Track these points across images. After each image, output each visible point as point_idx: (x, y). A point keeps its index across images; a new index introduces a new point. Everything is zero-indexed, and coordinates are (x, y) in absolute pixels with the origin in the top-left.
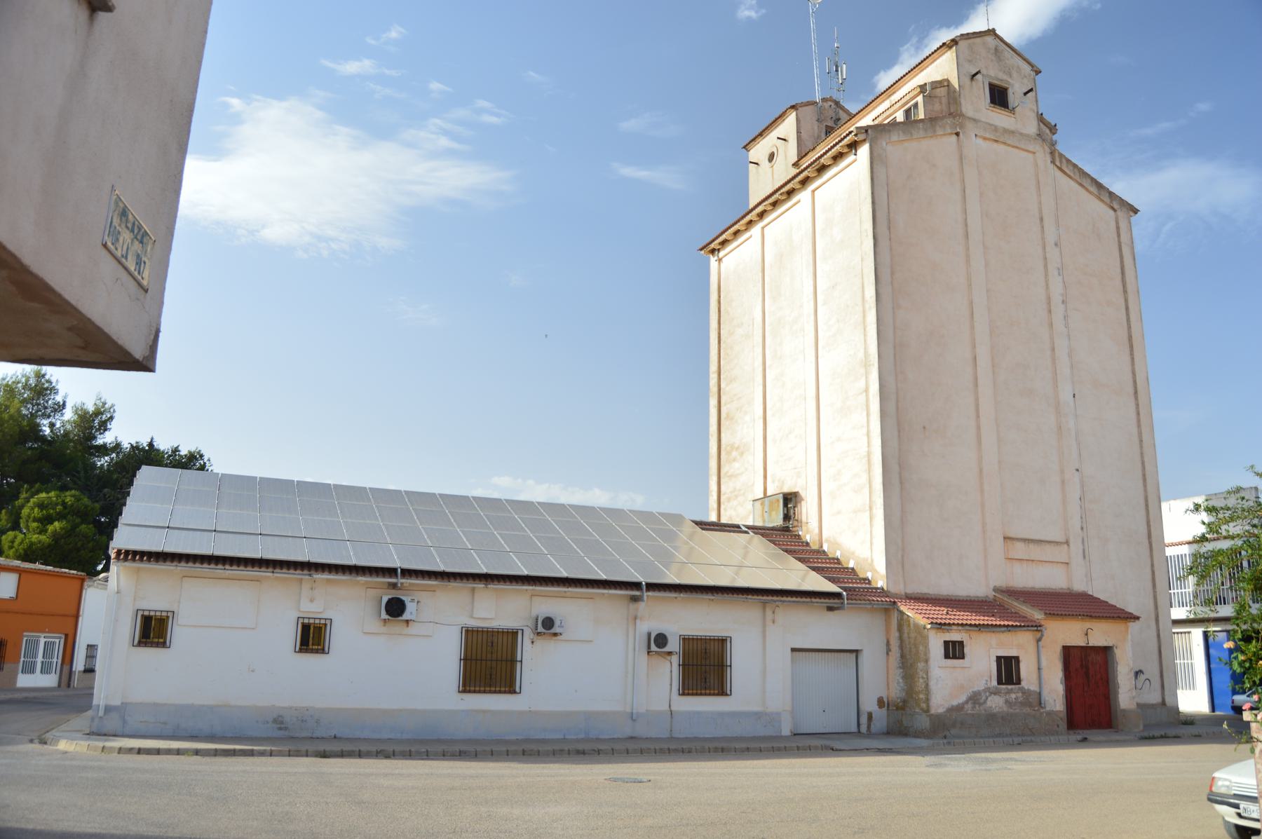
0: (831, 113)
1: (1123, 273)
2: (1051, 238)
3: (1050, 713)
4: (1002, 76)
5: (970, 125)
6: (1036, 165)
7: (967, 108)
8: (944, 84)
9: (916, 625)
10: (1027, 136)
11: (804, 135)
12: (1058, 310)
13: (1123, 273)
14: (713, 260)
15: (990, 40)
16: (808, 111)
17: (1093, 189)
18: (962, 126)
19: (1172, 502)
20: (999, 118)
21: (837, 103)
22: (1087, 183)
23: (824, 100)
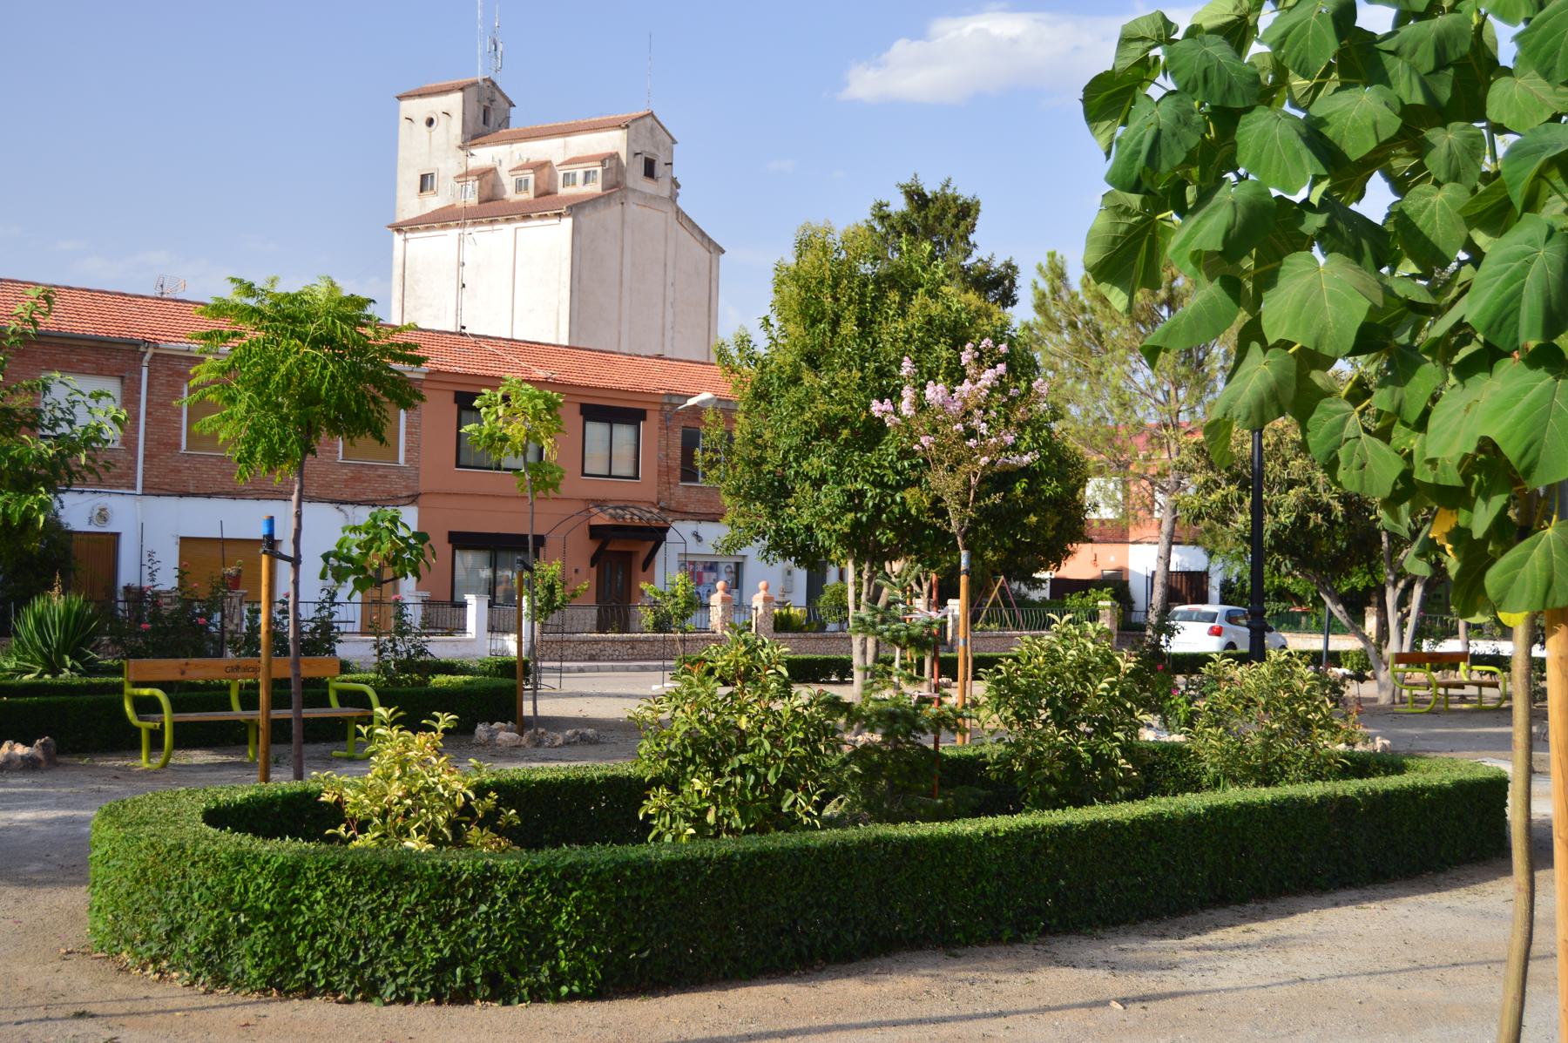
0: (488, 94)
1: (619, 696)
2: (669, 281)
3: (137, 595)
4: (654, 151)
5: (630, 195)
6: (666, 222)
7: (630, 182)
8: (614, 157)
9: (1425, 590)
10: (661, 198)
11: (467, 117)
12: (669, 334)
13: (619, 696)
14: (398, 238)
15: (649, 120)
16: (472, 91)
17: (699, 238)
18: (626, 197)
19: (594, 612)
20: (648, 186)
21: (494, 84)
22: (696, 233)
23: (484, 80)
